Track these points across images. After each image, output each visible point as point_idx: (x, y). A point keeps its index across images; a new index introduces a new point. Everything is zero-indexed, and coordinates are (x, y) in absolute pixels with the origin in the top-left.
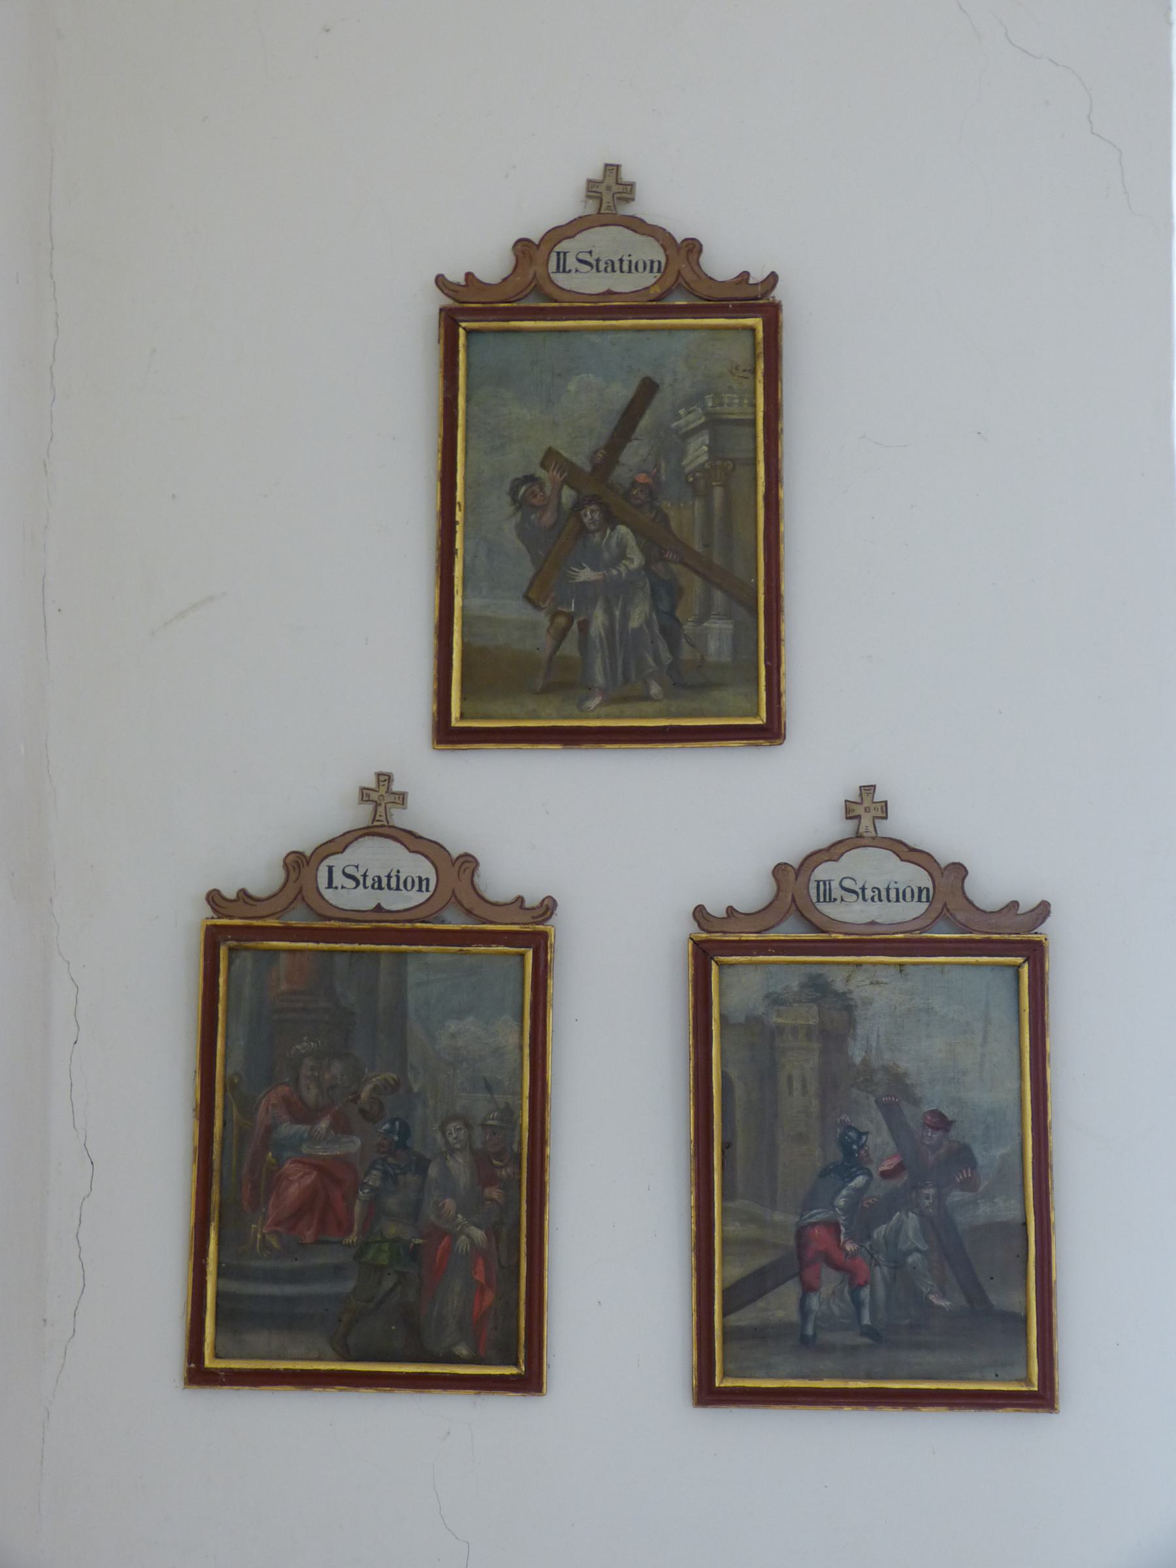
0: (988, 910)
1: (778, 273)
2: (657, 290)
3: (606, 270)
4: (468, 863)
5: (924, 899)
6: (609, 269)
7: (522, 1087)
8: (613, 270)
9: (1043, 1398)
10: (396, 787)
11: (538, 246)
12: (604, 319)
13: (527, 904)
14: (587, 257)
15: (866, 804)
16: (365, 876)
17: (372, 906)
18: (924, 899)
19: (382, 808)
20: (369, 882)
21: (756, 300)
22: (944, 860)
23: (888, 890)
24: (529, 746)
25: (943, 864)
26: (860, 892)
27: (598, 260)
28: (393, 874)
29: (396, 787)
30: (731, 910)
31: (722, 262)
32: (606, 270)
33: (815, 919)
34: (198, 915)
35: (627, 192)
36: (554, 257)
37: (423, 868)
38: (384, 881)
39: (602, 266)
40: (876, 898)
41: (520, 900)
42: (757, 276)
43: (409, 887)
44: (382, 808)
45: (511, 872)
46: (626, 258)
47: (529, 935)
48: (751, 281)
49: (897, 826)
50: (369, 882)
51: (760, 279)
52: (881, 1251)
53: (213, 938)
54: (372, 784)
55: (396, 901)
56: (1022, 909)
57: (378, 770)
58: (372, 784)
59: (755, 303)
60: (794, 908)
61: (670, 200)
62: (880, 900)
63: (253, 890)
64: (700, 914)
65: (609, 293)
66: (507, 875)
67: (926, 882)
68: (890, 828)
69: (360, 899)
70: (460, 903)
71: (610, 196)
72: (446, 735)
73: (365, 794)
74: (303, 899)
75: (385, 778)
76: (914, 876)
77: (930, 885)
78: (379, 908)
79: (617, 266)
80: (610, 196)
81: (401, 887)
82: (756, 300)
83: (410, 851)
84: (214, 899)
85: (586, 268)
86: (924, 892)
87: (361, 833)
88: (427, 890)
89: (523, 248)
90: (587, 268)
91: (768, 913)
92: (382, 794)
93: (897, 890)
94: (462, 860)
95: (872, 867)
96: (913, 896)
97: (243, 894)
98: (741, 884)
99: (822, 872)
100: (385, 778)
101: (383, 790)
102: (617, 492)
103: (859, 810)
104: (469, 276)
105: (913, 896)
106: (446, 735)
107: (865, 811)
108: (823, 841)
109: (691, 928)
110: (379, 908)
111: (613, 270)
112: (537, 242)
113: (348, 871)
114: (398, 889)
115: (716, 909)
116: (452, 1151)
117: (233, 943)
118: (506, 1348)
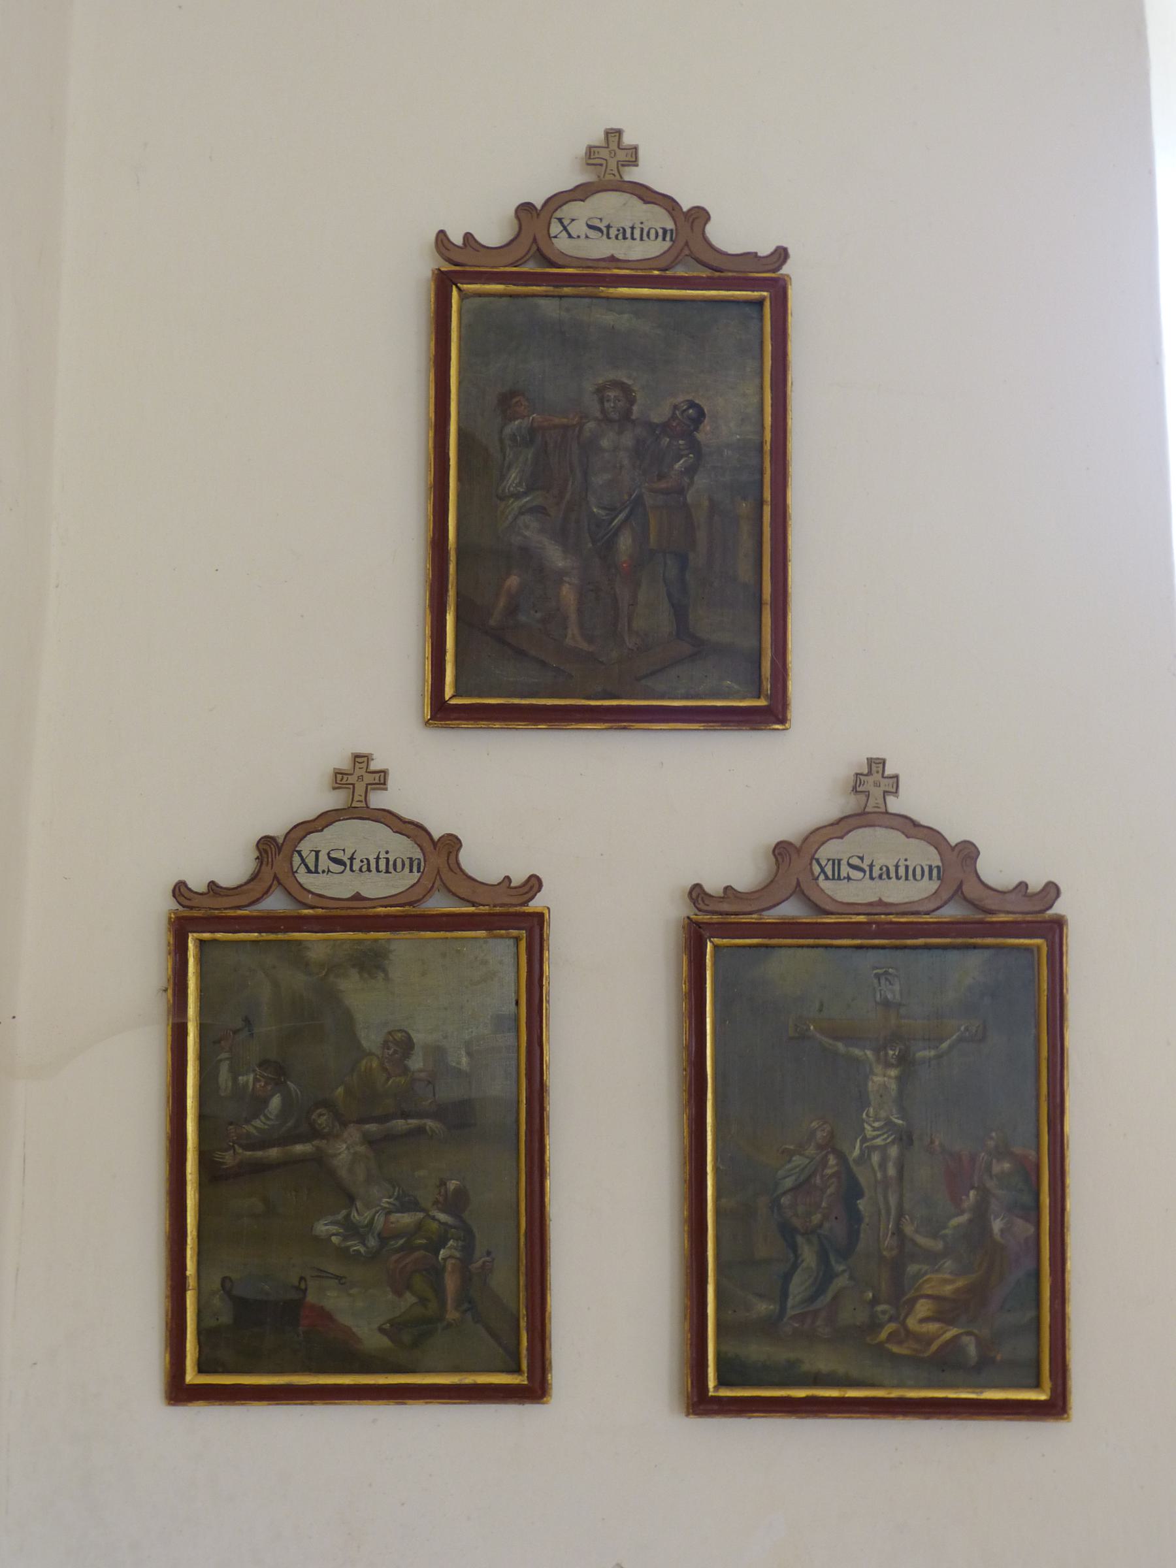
1: (790, 251)
3: (617, 237)
6: (620, 237)
8: (625, 238)
12: (526, 285)
14: (596, 223)
19: (358, 784)
22: (953, 840)
23: (897, 867)
24: (470, 724)
25: (436, 836)
28: (638, 226)
30: (212, 884)
32: (617, 237)
33: (815, 897)
34: (165, 905)
39: (613, 232)
40: (884, 876)
41: (1023, 885)
43: (918, 876)
44: (358, 784)
46: (638, 226)
54: (889, 771)
55: (898, 893)
60: (438, 882)
62: (889, 878)
64: (180, 890)
65: (613, 259)
66: (488, 859)
70: (803, 893)
72: (441, 713)
74: (280, 883)
76: (924, 855)
77: (421, 856)
80: (610, 164)
81: (391, 869)
83: (841, 837)
85: (597, 234)
91: (766, 892)
92: (358, 781)
93: (907, 867)
95: (881, 845)
98: (735, 866)
99: (828, 851)
100: (360, 759)
102: (605, 466)
103: (868, 786)
105: (419, 864)
106: (441, 713)
107: (872, 783)
108: (309, 813)
109: (173, 905)
111: (625, 238)
114: (387, 872)
115: (198, 883)
117: (206, 936)
118: (476, 1329)
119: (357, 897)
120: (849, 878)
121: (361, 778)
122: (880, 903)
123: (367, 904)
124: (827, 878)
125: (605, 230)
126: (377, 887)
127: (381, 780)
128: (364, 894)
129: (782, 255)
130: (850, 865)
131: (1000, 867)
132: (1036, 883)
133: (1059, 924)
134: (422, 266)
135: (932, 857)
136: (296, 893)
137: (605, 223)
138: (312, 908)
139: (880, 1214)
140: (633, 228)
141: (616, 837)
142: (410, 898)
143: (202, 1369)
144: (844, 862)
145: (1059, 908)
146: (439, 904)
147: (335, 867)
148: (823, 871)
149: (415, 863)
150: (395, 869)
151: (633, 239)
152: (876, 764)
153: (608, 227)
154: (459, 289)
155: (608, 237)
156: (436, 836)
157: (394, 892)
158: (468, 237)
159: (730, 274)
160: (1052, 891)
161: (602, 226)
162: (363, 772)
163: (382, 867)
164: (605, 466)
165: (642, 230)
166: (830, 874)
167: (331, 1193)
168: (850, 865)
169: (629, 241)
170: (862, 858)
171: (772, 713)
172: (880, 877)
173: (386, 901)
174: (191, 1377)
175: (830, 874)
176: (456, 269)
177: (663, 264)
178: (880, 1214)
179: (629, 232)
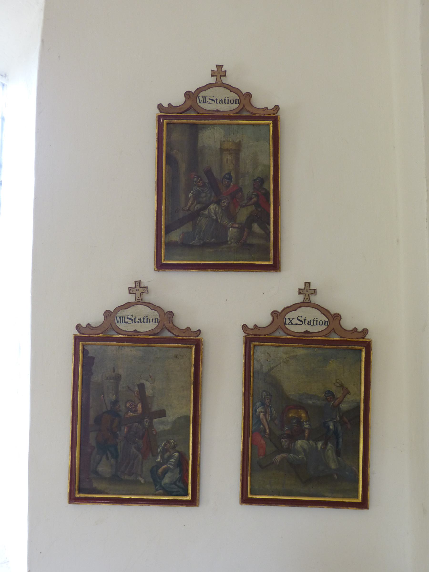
0: (343, 327)
2: (238, 110)
4: (337, 316)
5: (326, 324)
11: (193, 94)
13: (358, 331)
14: (212, 98)
15: (307, 294)
16: (305, 319)
18: (326, 324)
20: (307, 322)
21: (273, 117)
25: (332, 313)
26: (134, 319)
27: (217, 99)
31: (262, 101)
35: (224, 74)
36: (198, 98)
37: (155, 315)
38: (142, 320)
39: (218, 101)
50: (307, 322)
52: (313, 435)
53: (77, 339)
55: (311, 329)
59: (273, 116)
63: (260, 325)
67: (158, 317)
69: (299, 329)
73: (300, 291)
79: (223, 102)
82: (273, 117)
83: (296, 310)
84: (78, 327)
86: (157, 320)
87: (299, 305)
89: (188, 94)
90: (213, 102)
92: (139, 289)
94: (335, 316)
95: (141, 311)
96: (150, 320)
97: (256, 326)
104: (169, 105)
105: (150, 320)
107: (307, 291)
111: (222, 103)
114: (147, 322)
118: (175, 482)
119: (135, 331)
120: (127, 323)
121: (137, 290)
123: (310, 335)
126: (145, 328)
127: (146, 290)
129: (277, 108)
130: (128, 318)
131: (349, 323)
136: (287, 331)
138: (290, 335)
141: (222, 305)
142: (151, 333)
143: (187, 495)
145: (368, 337)
146: (167, 334)
147: (129, 321)
149: (157, 320)
150: (150, 322)
153: (217, 99)
155: (217, 103)
156: (332, 313)
157: (146, 330)
158: (169, 105)
159: (257, 115)
162: (305, 290)
164: (217, 181)
167: (121, 436)
168: (128, 318)
171: (275, 267)
172: (138, 322)
173: (146, 333)
174: (189, 498)
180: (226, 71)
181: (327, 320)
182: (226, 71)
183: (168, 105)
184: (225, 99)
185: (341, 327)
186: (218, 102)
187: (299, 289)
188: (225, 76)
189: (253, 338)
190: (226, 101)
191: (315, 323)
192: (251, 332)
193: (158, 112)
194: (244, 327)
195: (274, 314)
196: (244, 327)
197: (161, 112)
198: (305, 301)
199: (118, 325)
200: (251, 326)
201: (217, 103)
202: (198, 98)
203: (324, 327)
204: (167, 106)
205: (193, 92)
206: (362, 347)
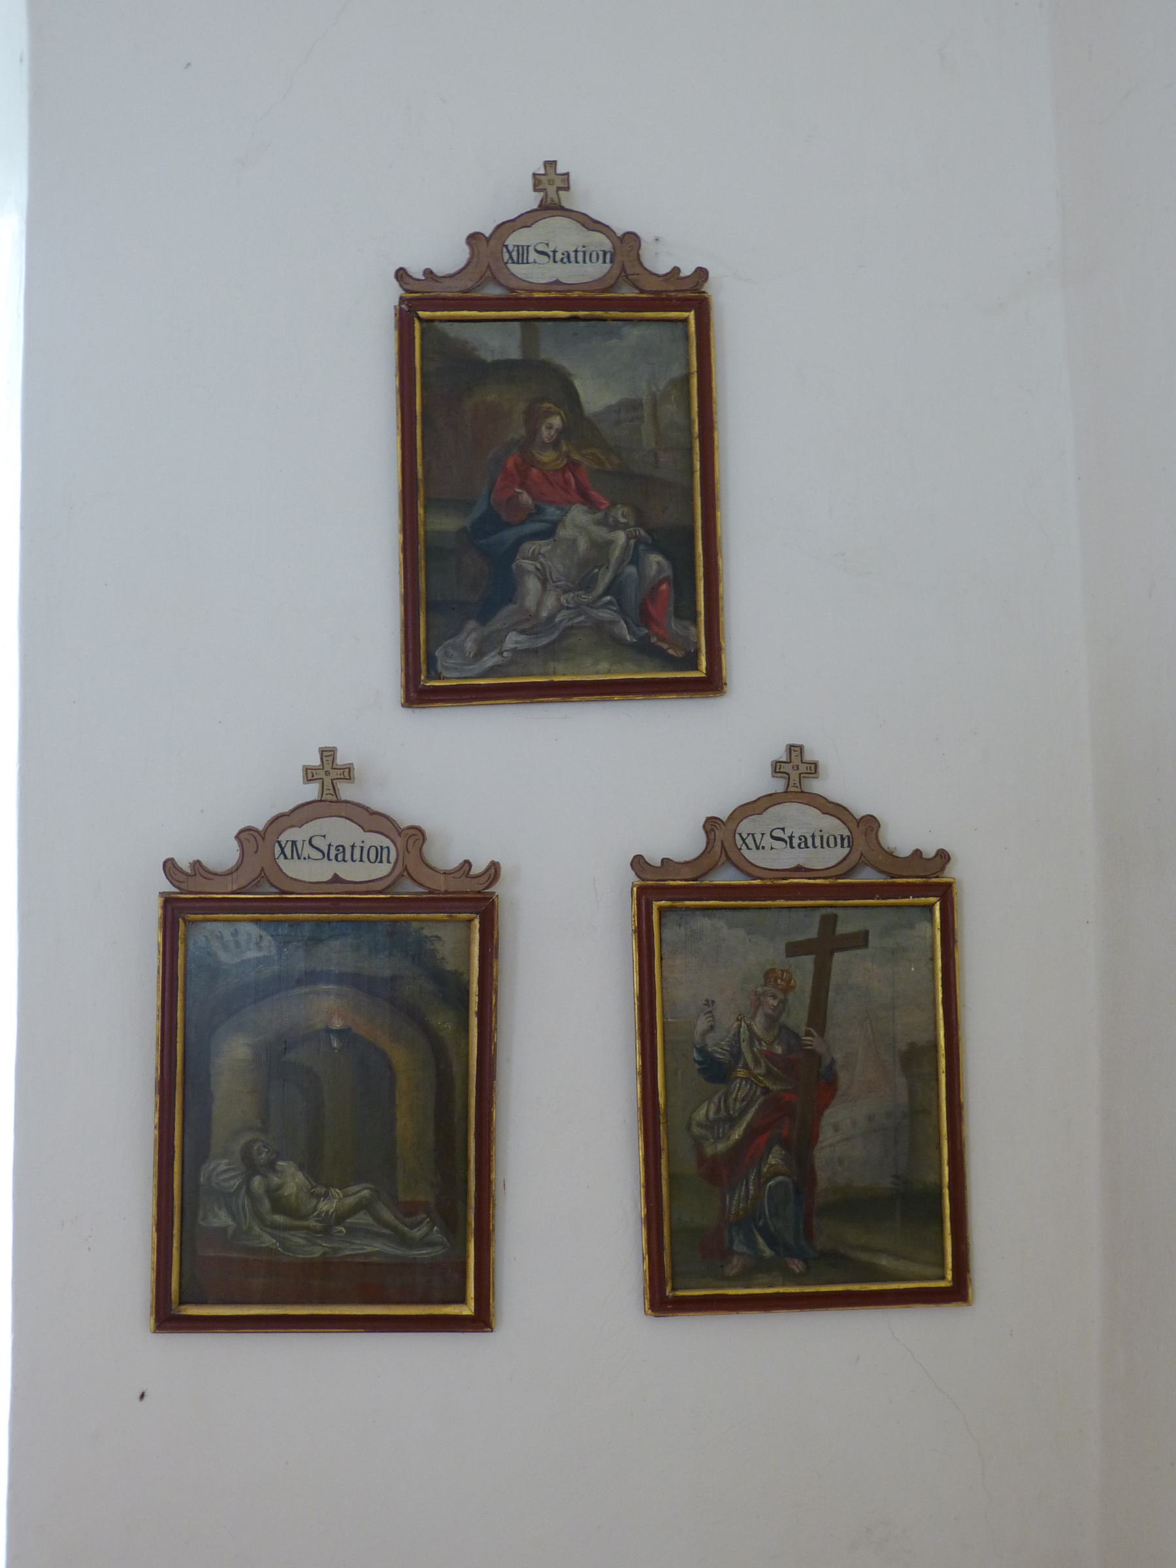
6: (803, 845)
7: (467, 1044)
9: (958, 1292)
10: (340, 760)
11: (488, 240)
17: (327, 877)
22: (404, 823)
27: (555, 252)
28: (817, 834)
29: (340, 760)
31: (904, 835)
36: (737, 836)
42: (687, 270)
45: (462, 837)
46: (817, 834)
47: (476, 900)
48: (682, 275)
49: (827, 786)
51: (689, 273)
55: (358, 872)
56: (476, 870)
57: (792, 743)
58: (316, 762)
61: (614, 195)
68: (816, 786)
69: (781, 858)
71: (552, 192)
75: (328, 754)
78: (336, 879)
82: (688, 298)
88: (388, 862)
92: (329, 770)
95: (560, 234)
101: (327, 767)
107: (795, 771)
110: (336, 879)
112: (487, 235)
113: (775, 834)
116: (742, 1078)
122: (557, 282)
124: (513, 262)
125: (551, 254)
128: (342, 875)
130: (773, 838)
132: (930, 851)
133: (949, 887)
134: (387, 298)
135: (607, 245)
136: (745, 867)
137: (788, 833)
139: (812, 1155)
140: (813, 837)
141: (562, 806)
143: (462, 1300)
144: (531, 249)
148: (511, 257)
151: (577, 262)
152: (795, 750)
153: (791, 838)
154: (420, 319)
155: (792, 847)
158: (428, 273)
160: (943, 857)
161: (549, 250)
163: (357, 856)
164: (553, 463)
165: (822, 837)
166: (515, 258)
167: (309, 1126)
169: (574, 264)
170: (783, 829)
174: (468, 1310)
175: (515, 258)
176: (421, 306)
177: (835, 872)
178: (812, 1155)
179: (572, 255)
180: (567, 174)
181: (846, 833)
182: (567, 174)
183: (663, 860)
184: (813, 837)
185: (879, 843)
186: (553, 261)
187: (534, 175)
188: (567, 189)
189: (662, 897)
190: (818, 842)
191: (357, 856)
192: (416, 287)
193: (631, 877)
194: (401, 275)
195: (711, 825)
196: (401, 275)
197: (407, 291)
198: (791, 789)
199: (281, 862)
200: (416, 272)
201: (792, 847)
202: (737, 836)
203: (841, 852)
204: (659, 864)
205: (487, 235)
206: (932, 899)
